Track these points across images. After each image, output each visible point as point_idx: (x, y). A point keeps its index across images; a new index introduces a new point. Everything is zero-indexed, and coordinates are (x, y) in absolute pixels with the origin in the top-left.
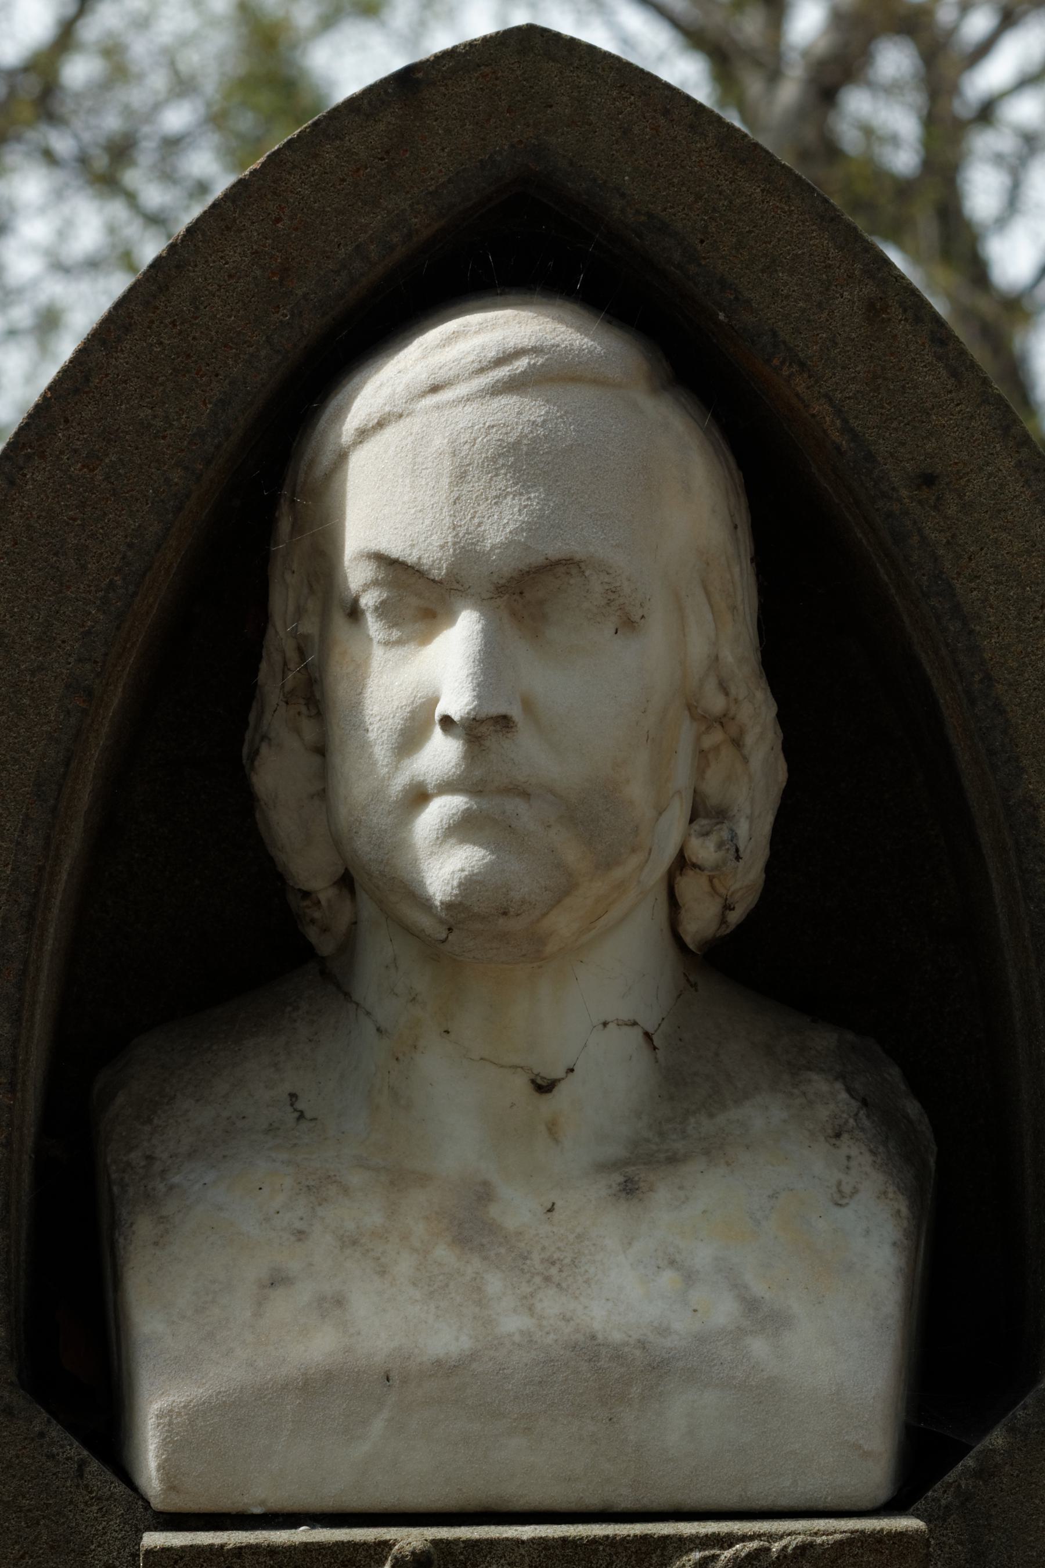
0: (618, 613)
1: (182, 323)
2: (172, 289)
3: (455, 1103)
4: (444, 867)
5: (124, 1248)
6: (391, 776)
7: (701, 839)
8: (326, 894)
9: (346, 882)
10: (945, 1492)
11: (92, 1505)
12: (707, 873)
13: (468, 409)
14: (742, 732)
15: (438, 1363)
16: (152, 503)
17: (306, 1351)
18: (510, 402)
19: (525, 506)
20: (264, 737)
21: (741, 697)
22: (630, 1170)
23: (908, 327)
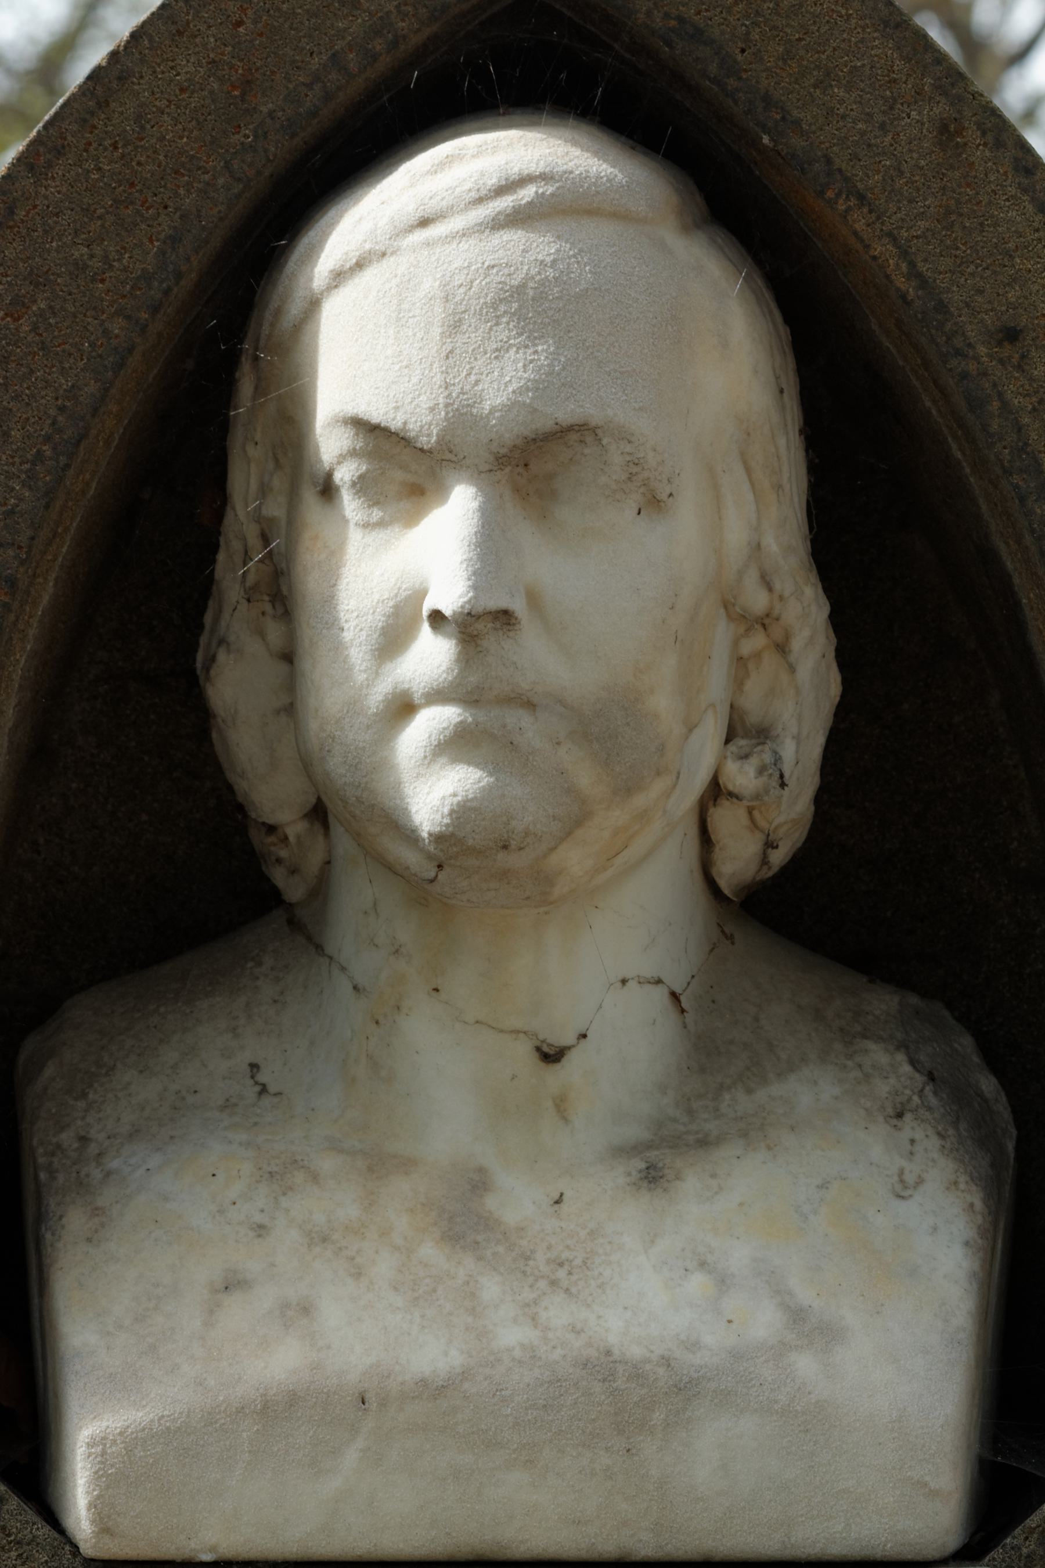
0: (642, 490)
1: (125, 146)
2: (113, 105)
3: (444, 1070)
4: (432, 789)
5: (52, 1245)
6: (370, 684)
7: (738, 763)
8: (295, 829)
9: (319, 814)
10: (1026, 1538)
11: (10, 1551)
12: (745, 803)
13: (464, 245)
14: (788, 637)
15: (423, 1383)
16: (88, 359)
17: (266, 1368)
18: (514, 238)
19: (531, 362)
20: (222, 642)
21: (786, 594)
22: (653, 1154)
23: (988, 153)
